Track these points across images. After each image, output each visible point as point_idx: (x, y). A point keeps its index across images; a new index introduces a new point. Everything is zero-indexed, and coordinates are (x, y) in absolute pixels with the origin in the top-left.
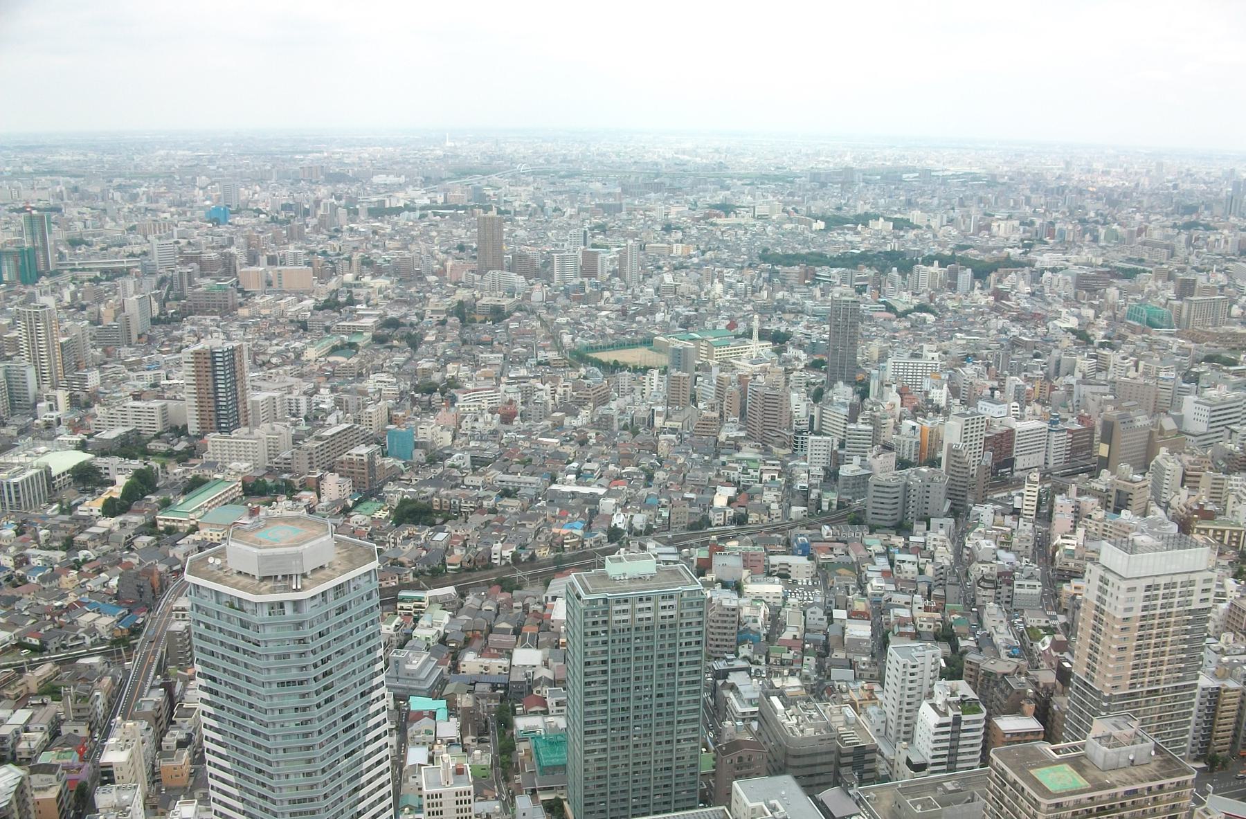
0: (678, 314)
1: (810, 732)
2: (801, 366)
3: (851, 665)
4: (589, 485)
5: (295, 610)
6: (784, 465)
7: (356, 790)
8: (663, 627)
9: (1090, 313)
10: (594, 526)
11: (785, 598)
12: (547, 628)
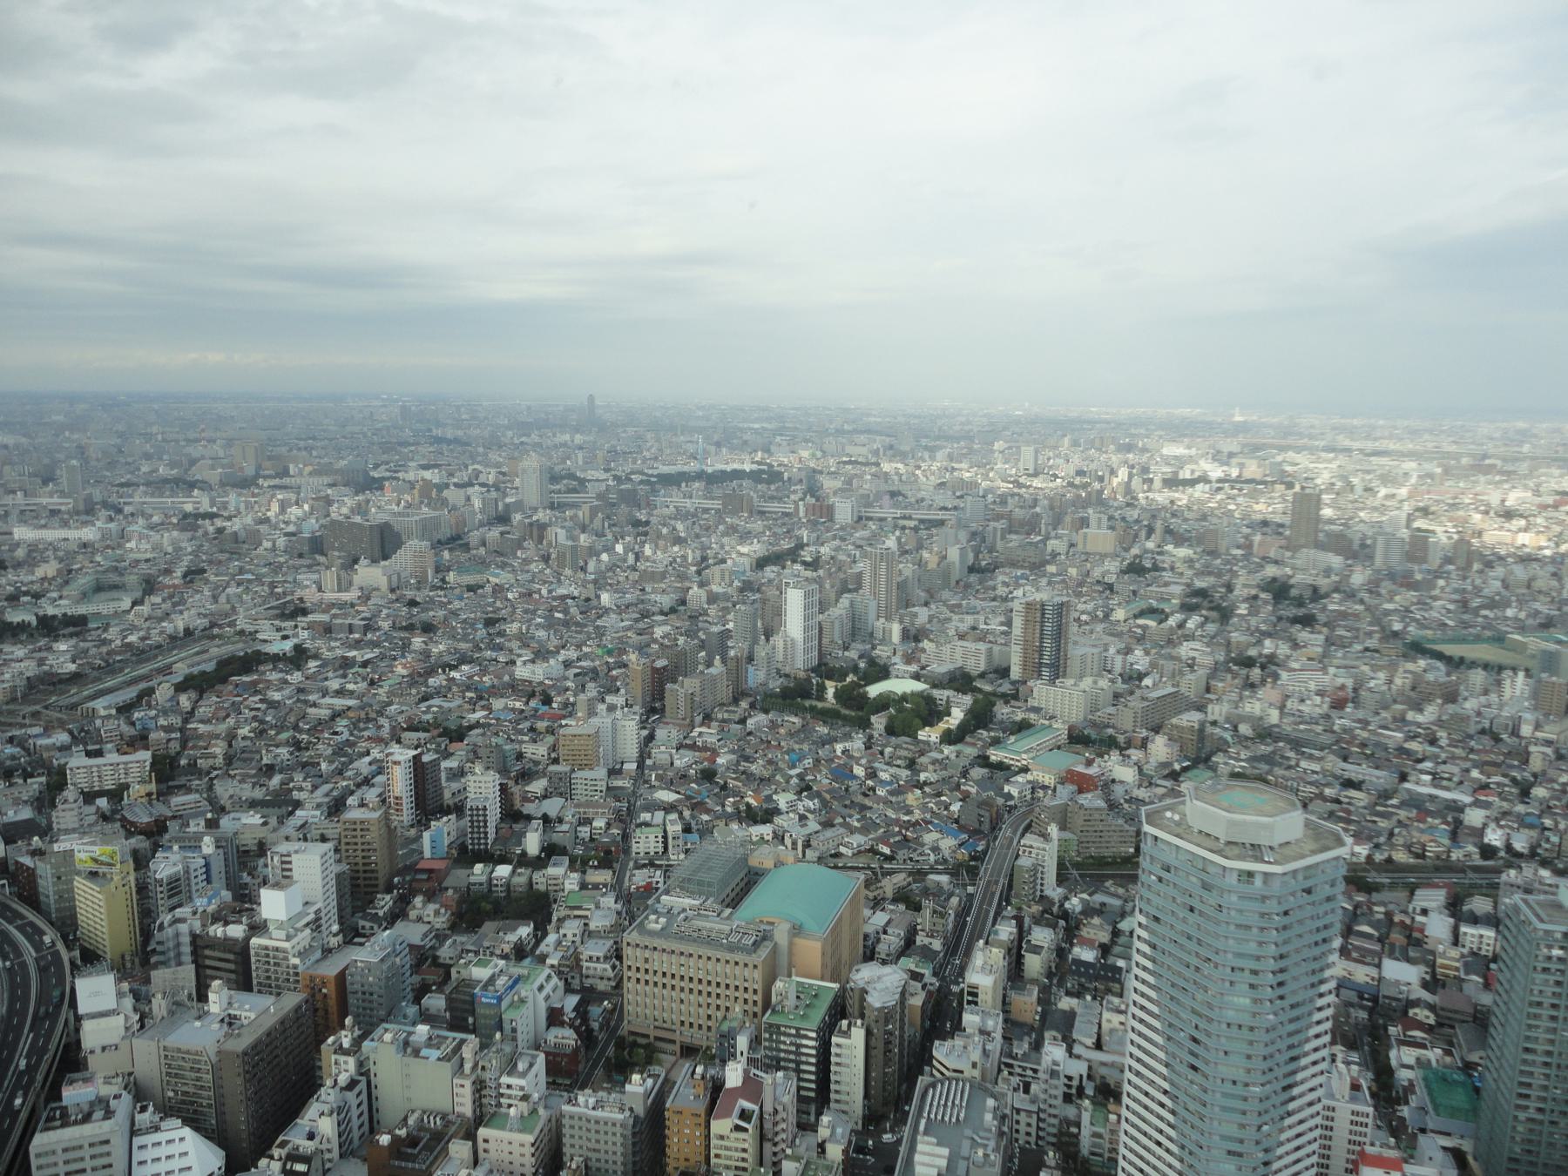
0: (1537, 612)
5: (1265, 883)
7: (1290, 1087)
10: (1461, 837)
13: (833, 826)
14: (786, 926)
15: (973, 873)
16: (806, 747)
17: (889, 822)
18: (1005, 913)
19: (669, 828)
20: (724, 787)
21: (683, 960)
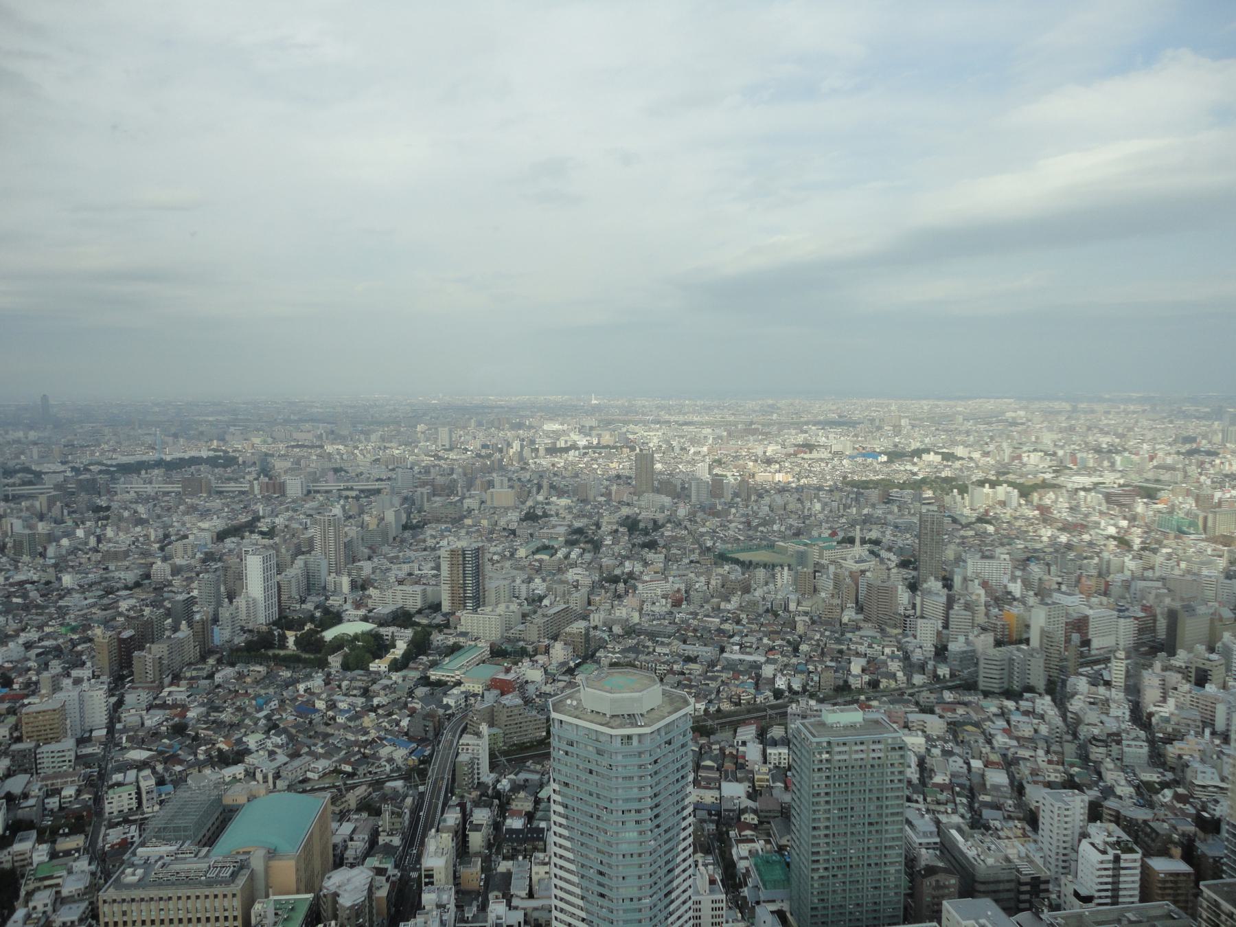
0: (791, 526)
1: (990, 861)
2: (894, 565)
3: (997, 807)
4: (750, 654)
6: (899, 642)
7: (670, 893)
8: (872, 766)
9: (1124, 523)
11: (928, 750)
12: (742, 767)
13: (300, 756)
14: (261, 853)
15: (423, 774)
16: (271, 691)
17: (350, 744)
18: (451, 803)
19: (143, 784)
20: (196, 738)
21: (162, 905)
